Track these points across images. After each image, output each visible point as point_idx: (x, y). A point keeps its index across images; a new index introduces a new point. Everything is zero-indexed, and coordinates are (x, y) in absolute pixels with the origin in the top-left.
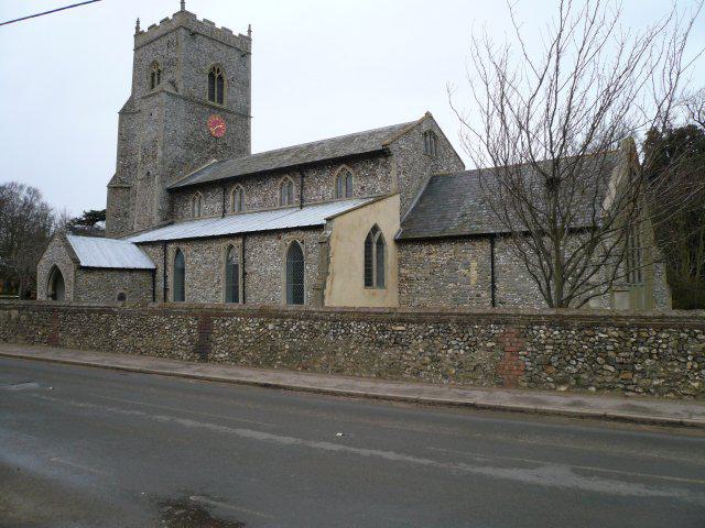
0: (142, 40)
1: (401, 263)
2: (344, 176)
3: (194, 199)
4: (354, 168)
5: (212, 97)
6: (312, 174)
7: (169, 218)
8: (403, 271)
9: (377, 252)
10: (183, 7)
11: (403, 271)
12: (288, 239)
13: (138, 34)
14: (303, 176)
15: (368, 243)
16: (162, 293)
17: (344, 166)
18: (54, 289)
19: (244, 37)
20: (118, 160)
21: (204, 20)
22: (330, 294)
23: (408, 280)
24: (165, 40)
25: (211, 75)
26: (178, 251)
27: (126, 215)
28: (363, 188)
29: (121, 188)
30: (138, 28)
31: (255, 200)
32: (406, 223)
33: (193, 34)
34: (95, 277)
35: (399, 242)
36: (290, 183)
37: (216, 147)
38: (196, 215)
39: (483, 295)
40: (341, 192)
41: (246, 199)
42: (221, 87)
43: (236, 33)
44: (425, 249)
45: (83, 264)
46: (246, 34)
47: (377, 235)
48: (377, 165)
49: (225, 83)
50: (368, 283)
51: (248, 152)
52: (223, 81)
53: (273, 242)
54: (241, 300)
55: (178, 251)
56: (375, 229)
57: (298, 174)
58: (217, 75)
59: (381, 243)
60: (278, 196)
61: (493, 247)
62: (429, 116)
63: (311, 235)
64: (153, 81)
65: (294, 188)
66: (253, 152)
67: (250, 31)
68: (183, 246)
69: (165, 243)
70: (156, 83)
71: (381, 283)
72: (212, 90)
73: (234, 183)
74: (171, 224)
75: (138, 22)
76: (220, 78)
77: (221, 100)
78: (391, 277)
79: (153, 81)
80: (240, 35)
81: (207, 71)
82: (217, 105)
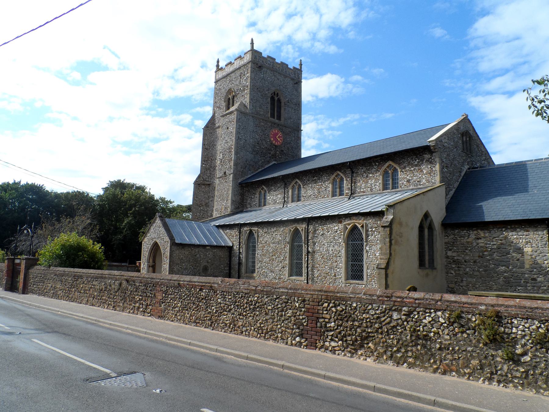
0: (221, 74)
1: (449, 246)
2: (297, 187)
3: (293, 186)
4: (399, 164)
5: (273, 116)
6: (361, 170)
7: (240, 207)
8: (450, 253)
9: (429, 235)
10: (253, 46)
11: (450, 253)
12: (349, 223)
13: (219, 69)
14: (353, 172)
15: (421, 228)
16: (237, 267)
17: (391, 163)
18: (154, 261)
19: (297, 69)
20: (202, 164)
21: (268, 57)
22: (392, 273)
23: (457, 262)
24: (238, 73)
25: (272, 98)
26: (251, 232)
27: (207, 205)
28: (408, 181)
29: (204, 185)
30: (218, 66)
31: (310, 192)
32: (450, 207)
33: (260, 67)
34: (186, 252)
35: (446, 225)
36: (342, 180)
37: (276, 153)
38: (262, 204)
39: (539, 279)
40: (336, 192)
41: (303, 191)
42: (279, 108)
43: (291, 66)
44: (473, 234)
45: (177, 241)
46: (298, 67)
47: (428, 222)
48: (422, 160)
49: (283, 104)
50: (422, 264)
51: (297, 159)
52: (280, 103)
53: (337, 227)
54: (304, 274)
55: (251, 232)
56: (426, 216)
57: (349, 171)
58: (276, 98)
59: (431, 228)
60: (330, 189)
61: (240, 233)
62: (466, 121)
63: (370, 222)
64: (229, 104)
65: (345, 182)
66: (302, 157)
67: (301, 65)
68: (255, 229)
69: (240, 226)
70: (231, 105)
71: (432, 266)
72: (273, 109)
73: (294, 179)
74: (242, 212)
75: (218, 62)
76: (279, 100)
77: (279, 118)
78: (439, 261)
79: (229, 104)
80: (294, 68)
81: (269, 95)
82: (277, 121)
